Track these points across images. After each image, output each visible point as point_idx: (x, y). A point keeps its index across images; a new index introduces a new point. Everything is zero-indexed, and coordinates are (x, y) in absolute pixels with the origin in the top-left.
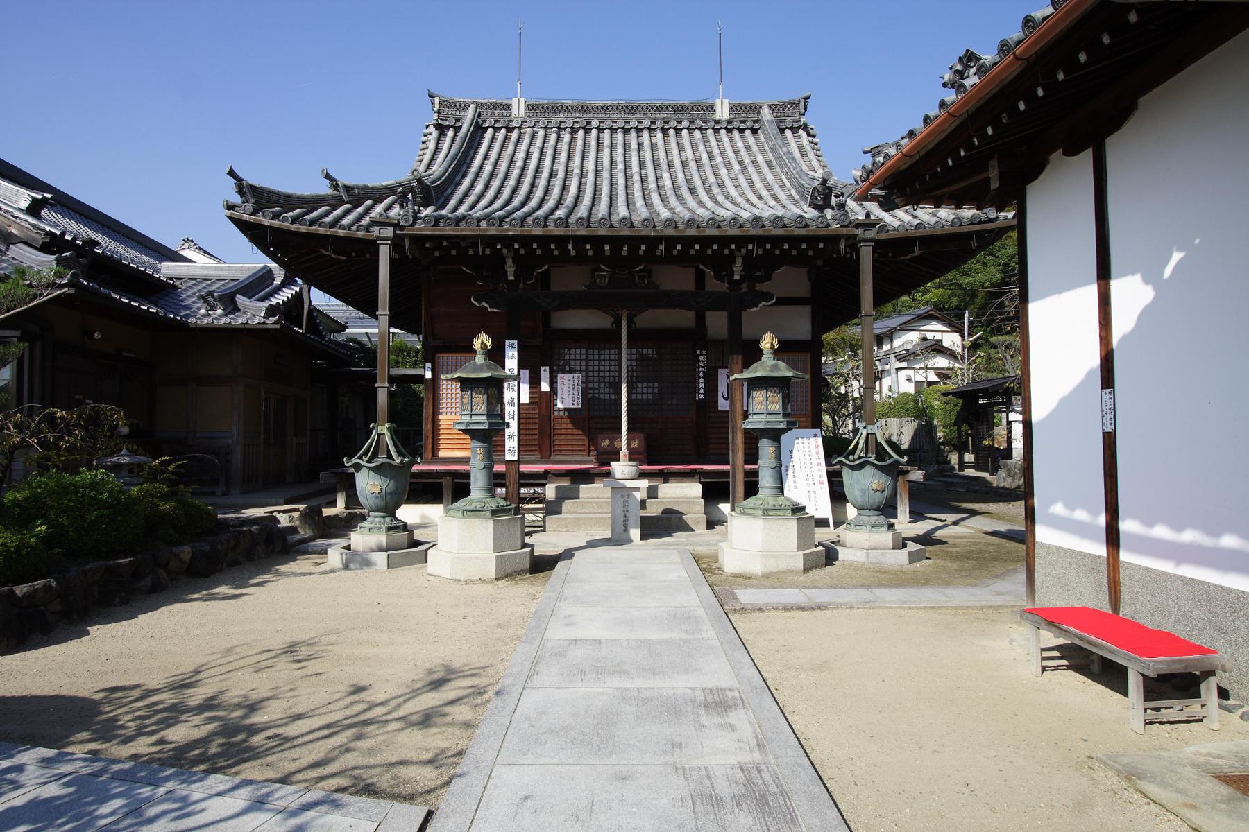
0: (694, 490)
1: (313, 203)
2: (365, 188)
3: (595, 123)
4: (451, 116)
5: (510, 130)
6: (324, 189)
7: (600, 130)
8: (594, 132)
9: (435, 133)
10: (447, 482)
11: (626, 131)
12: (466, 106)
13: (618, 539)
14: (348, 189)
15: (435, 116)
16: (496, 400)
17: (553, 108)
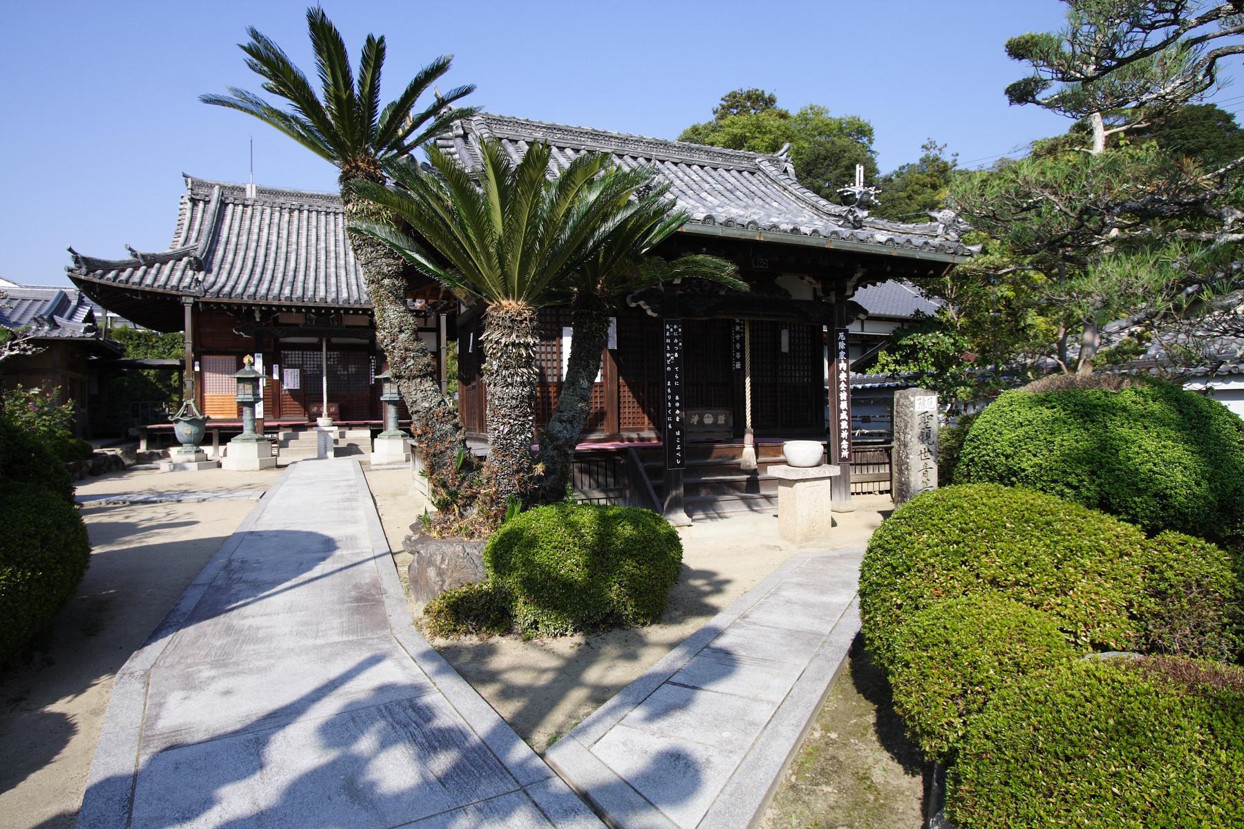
0: (366, 433)
1: (121, 267)
2: (154, 255)
3: (306, 207)
4: (202, 192)
5: (245, 206)
6: (128, 257)
7: (309, 211)
8: (306, 213)
9: (189, 205)
10: (215, 432)
11: (327, 213)
12: (212, 186)
13: (322, 456)
14: (143, 257)
15: (189, 192)
16: (256, 387)
17: (276, 193)
